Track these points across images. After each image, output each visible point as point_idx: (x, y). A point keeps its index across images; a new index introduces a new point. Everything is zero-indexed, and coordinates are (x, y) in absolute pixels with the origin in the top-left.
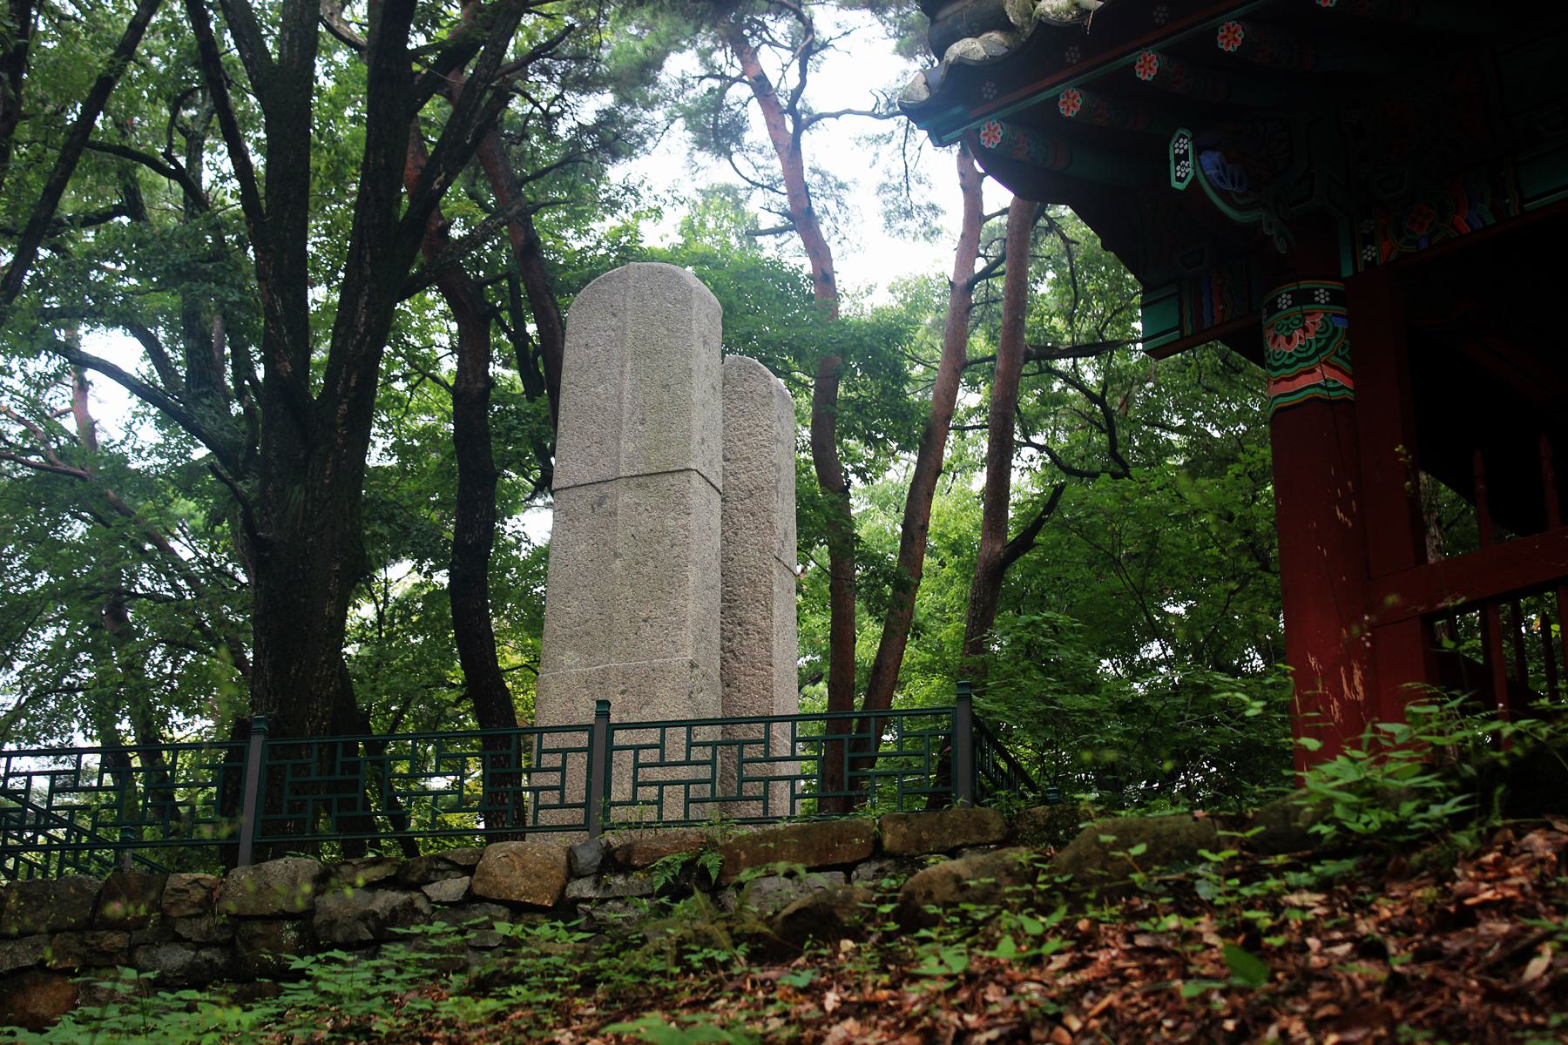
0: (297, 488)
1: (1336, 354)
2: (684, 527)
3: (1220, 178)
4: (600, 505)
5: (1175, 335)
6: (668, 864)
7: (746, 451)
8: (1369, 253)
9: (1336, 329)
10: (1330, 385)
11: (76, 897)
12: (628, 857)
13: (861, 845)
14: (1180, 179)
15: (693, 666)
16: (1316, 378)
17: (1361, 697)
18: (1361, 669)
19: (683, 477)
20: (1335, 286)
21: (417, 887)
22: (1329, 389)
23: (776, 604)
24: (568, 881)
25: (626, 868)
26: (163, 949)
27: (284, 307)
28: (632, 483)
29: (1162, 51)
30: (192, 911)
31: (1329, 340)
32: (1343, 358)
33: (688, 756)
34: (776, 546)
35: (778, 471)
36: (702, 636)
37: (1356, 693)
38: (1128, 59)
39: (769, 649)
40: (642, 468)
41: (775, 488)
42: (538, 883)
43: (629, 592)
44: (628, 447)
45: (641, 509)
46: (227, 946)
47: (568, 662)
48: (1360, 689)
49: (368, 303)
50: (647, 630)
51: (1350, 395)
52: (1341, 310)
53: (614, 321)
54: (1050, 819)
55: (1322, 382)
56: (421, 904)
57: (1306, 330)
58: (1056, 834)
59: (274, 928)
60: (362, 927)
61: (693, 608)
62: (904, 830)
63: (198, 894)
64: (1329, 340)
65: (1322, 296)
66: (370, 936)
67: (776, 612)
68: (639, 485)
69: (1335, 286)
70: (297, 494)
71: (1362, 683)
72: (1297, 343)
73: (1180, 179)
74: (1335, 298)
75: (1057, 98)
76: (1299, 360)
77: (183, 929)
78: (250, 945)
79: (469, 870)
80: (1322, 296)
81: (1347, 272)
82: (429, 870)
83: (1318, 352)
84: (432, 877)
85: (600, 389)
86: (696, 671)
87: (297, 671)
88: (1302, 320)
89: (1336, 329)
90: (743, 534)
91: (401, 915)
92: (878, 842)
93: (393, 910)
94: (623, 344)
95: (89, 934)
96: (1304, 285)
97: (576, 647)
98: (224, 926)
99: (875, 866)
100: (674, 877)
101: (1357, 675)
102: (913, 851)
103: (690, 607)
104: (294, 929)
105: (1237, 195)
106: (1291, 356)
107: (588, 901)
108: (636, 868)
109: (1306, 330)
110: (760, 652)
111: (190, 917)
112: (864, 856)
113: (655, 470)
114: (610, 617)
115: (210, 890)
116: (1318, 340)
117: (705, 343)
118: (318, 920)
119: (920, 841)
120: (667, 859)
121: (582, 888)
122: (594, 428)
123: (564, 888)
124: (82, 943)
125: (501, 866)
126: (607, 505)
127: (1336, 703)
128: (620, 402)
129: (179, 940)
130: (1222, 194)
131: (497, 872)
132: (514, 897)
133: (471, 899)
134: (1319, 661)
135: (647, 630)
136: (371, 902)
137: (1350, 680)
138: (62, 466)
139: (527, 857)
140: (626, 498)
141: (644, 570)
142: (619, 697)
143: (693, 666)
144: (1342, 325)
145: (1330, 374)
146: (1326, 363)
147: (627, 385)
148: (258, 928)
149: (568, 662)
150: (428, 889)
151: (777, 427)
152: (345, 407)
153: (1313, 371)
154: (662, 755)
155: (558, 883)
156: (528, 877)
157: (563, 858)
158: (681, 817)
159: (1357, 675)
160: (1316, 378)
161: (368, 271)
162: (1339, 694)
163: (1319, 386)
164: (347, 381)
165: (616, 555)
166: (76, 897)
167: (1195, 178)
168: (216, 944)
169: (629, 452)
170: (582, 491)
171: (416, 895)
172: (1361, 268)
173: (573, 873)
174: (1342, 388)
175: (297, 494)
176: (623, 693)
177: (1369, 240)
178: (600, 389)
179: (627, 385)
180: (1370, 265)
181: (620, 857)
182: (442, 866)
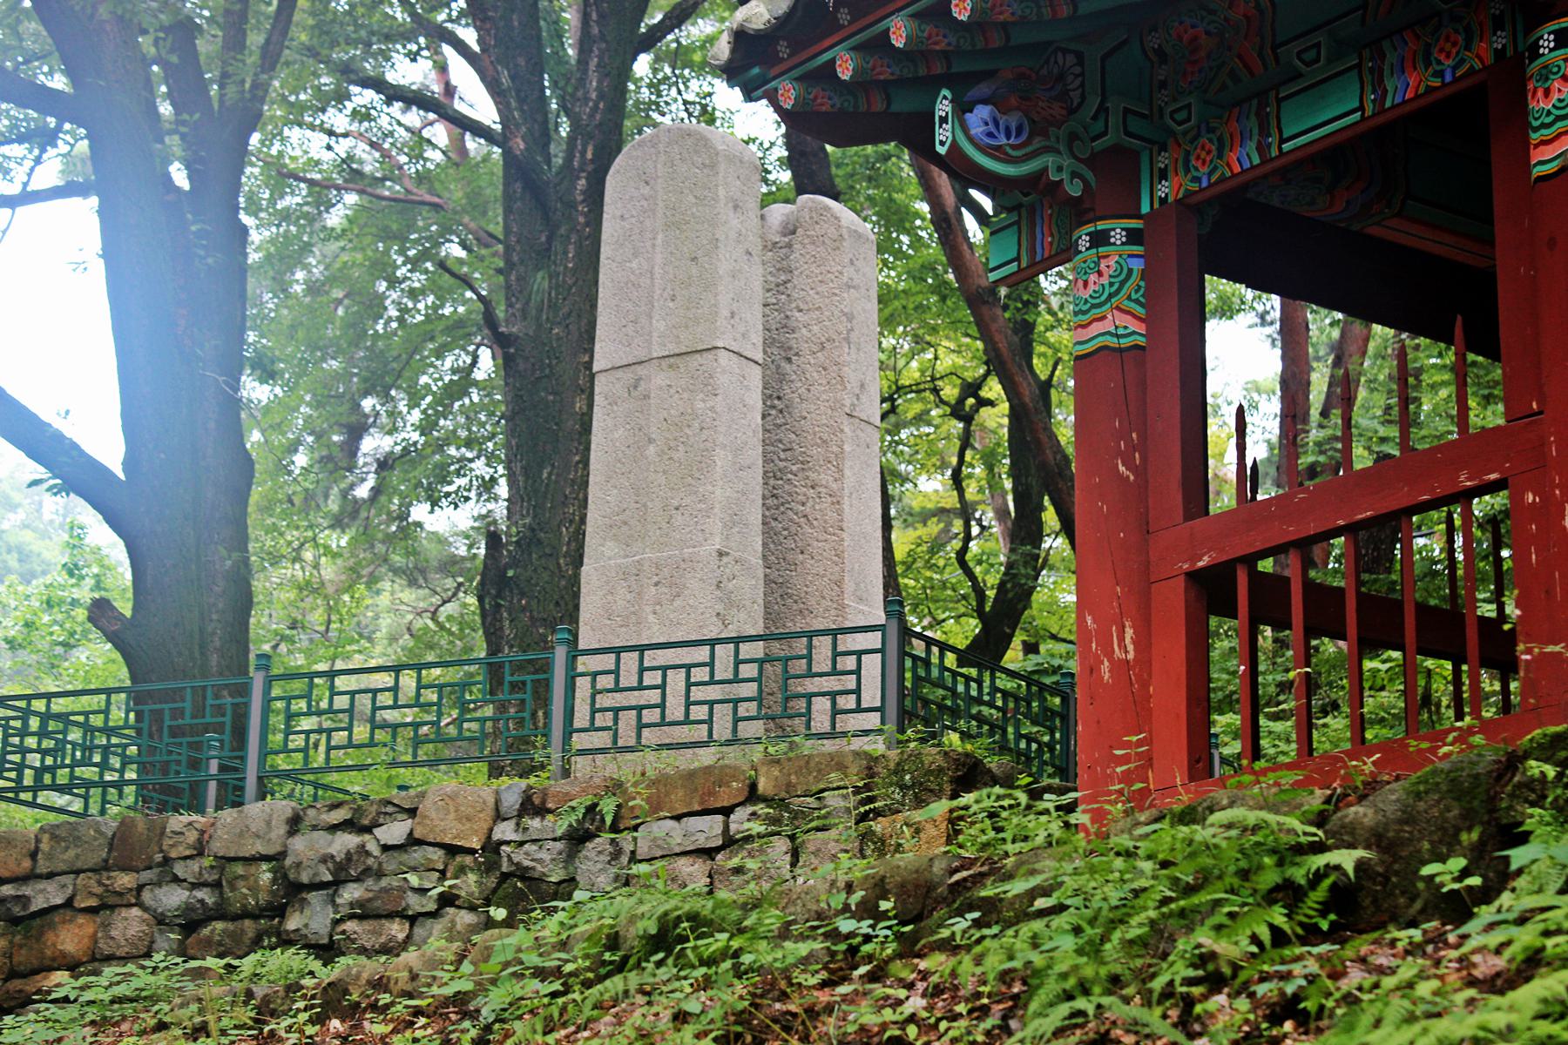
0: (540, 275)
1: (1129, 298)
2: (712, 409)
3: (990, 135)
4: (635, 387)
5: (1013, 267)
6: (573, 808)
7: (818, 301)
8: (1163, 189)
9: (1130, 271)
10: (1121, 331)
11: (95, 839)
12: (544, 802)
13: (738, 789)
14: (942, 143)
15: (721, 554)
16: (1106, 326)
17: (1131, 656)
18: (1133, 627)
19: (709, 355)
20: (1134, 224)
21: (368, 830)
22: (1117, 336)
23: (848, 464)
24: (495, 822)
25: (542, 812)
26: (165, 888)
27: (513, 78)
28: (665, 363)
29: (914, 16)
30: (188, 853)
31: (1123, 283)
32: (1137, 301)
33: (664, 677)
34: (848, 402)
35: (850, 320)
36: (734, 520)
37: (1126, 652)
38: (881, 26)
39: (840, 513)
40: (673, 348)
41: (847, 340)
42: (468, 825)
43: (662, 479)
44: (659, 325)
45: (672, 391)
46: (217, 885)
47: (608, 553)
48: (1130, 648)
49: (598, 66)
50: (679, 519)
51: (1141, 341)
52: (1138, 249)
53: (646, 190)
54: (898, 764)
55: (1112, 329)
56: (372, 847)
57: (1100, 274)
58: (902, 778)
59: (252, 869)
60: (322, 868)
61: (720, 493)
62: (776, 773)
63: (192, 837)
64: (1123, 283)
65: (1118, 236)
66: (330, 878)
67: (847, 472)
68: (670, 366)
69: (1134, 224)
70: (540, 281)
71: (1134, 642)
72: (1091, 287)
73: (942, 143)
74: (1133, 237)
75: (833, 61)
76: (1094, 306)
77: (179, 869)
78: (233, 888)
79: (412, 812)
80: (1118, 236)
81: (1145, 209)
82: (379, 813)
83: (1111, 296)
84: (381, 820)
85: (634, 265)
86: (725, 559)
87: (550, 474)
88: (1097, 264)
89: (1130, 271)
90: (815, 389)
91: (355, 857)
92: (753, 786)
93: (348, 853)
94: (654, 211)
95: (105, 874)
96: (1101, 226)
97: (615, 538)
98: (212, 867)
99: (750, 809)
100: (578, 821)
101: (1129, 633)
102: (783, 794)
103: (718, 492)
104: (269, 871)
105: (1014, 147)
106: (1086, 301)
107: (508, 843)
108: (550, 811)
109: (1100, 274)
110: (832, 516)
111: (186, 858)
112: (741, 799)
113: (684, 350)
114: (645, 505)
115: (202, 832)
116: (1111, 284)
117: (736, 207)
118: (288, 862)
119: (789, 784)
120: (574, 803)
121: (505, 831)
122: (630, 305)
123: (491, 830)
124: (100, 883)
125: (437, 809)
126: (643, 386)
127: (1106, 663)
128: (652, 279)
129: (176, 880)
130: (995, 152)
131: (433, 815)
132: (447, 841)
133: (413, 841)
134: (1094, 621)
135: (679, 519)
136: (330, 845)
137: (1121, 639)
138: (423, 194)
139: (460, 800)
140: (658, 379)
141: (676, 456)
142: (653, 589)
143: (721, 554)
144: (1137, 265)
145: (1122, 320)
146: (1118, 308)
147: (659, 259)
148: (239, 869)
149: (608, 553)
150: (376, 831)
151: (849, 272)
152: (583, 182)
153: (1103, 318)
154: (617, 681)
155: (486, 826)
156: (459, 820)
157: (491, 800)
158: (864, 657)
159: (1129, 633)
160: (1106, 326)
161: (595, 31)
162: (1110, 653)
163: (1109, 333)
164: (583, 153)
165: (651, 441)
166: (95, 839)
167: (954, 142)
168: (205, 884)
169: (661, 336)
170: (619, 373)
171: (367, 837)
172: (1156, 205)
173: (499, 817)
174: (1134, 333)
175: (540, 281)
176: (656, 584)
177: (1163, 175)
178: (634, 265)
179: (659, 259)
180: (1163, 201)
181: (537, 801)
182: (390, 809)
